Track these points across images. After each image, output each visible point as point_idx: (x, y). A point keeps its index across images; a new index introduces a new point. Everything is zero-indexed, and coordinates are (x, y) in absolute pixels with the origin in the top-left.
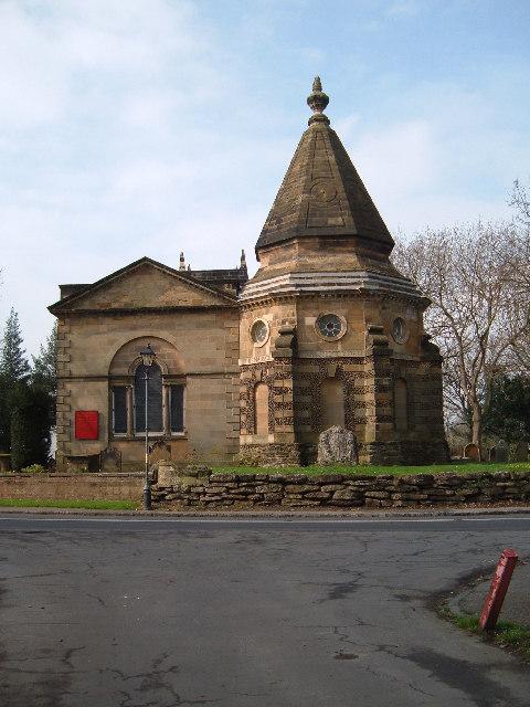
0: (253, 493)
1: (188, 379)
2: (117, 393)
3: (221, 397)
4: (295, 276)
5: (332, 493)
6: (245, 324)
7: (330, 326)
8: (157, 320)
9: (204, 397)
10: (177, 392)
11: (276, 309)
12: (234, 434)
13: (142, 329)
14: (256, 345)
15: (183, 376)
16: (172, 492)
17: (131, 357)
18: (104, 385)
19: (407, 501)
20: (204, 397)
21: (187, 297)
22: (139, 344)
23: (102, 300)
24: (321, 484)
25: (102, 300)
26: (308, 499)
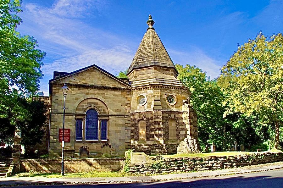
0: (182, 166)
1: (110, 117)
2: (79, 121)
3: (122, 125)
4: (158, 79)
5: (213, 164)
6: (135, 95)
7: (170, 99)
8: (97, 91)
9: (116, 125)
10: (104, 122)
11: (151, 91)
12: (129, 141)
13: (92, 93)
14: (140, 105)
15: (108, 116)
16: (143, 167)
17: (85, 106)
18: (72, 118)
19: (238, 166)
20: (116, 125)
21: (110, 84)
22: (89, 101)
23: (72, 81)
24: (209, 160)
25: (72, 81)
26: (204, 167)
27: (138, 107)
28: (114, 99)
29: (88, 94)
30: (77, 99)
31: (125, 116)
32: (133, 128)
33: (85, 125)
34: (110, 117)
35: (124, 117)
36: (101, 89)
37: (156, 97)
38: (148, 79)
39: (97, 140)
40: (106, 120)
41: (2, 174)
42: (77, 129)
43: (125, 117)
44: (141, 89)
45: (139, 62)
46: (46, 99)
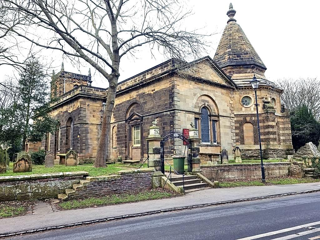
27: (243, 109)
28: (222, 98)
29: (202, 90)
30: (195, 95)
31: (230, 117)
32: (237, 131)
33: (209, 125)
34: (220, 118)
35: (229, 118)
36: (212, 86)
37: (264, 99)
38: (243, 79)
39: (209, 144)
40: (216, 121)
41: (193, 179)
42: (209, 130)
43: (231, 118)
44: (267, 88)
45: (234, 58)
46: (98, 91)
